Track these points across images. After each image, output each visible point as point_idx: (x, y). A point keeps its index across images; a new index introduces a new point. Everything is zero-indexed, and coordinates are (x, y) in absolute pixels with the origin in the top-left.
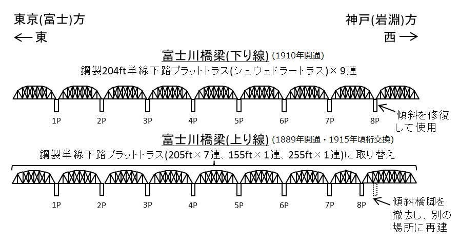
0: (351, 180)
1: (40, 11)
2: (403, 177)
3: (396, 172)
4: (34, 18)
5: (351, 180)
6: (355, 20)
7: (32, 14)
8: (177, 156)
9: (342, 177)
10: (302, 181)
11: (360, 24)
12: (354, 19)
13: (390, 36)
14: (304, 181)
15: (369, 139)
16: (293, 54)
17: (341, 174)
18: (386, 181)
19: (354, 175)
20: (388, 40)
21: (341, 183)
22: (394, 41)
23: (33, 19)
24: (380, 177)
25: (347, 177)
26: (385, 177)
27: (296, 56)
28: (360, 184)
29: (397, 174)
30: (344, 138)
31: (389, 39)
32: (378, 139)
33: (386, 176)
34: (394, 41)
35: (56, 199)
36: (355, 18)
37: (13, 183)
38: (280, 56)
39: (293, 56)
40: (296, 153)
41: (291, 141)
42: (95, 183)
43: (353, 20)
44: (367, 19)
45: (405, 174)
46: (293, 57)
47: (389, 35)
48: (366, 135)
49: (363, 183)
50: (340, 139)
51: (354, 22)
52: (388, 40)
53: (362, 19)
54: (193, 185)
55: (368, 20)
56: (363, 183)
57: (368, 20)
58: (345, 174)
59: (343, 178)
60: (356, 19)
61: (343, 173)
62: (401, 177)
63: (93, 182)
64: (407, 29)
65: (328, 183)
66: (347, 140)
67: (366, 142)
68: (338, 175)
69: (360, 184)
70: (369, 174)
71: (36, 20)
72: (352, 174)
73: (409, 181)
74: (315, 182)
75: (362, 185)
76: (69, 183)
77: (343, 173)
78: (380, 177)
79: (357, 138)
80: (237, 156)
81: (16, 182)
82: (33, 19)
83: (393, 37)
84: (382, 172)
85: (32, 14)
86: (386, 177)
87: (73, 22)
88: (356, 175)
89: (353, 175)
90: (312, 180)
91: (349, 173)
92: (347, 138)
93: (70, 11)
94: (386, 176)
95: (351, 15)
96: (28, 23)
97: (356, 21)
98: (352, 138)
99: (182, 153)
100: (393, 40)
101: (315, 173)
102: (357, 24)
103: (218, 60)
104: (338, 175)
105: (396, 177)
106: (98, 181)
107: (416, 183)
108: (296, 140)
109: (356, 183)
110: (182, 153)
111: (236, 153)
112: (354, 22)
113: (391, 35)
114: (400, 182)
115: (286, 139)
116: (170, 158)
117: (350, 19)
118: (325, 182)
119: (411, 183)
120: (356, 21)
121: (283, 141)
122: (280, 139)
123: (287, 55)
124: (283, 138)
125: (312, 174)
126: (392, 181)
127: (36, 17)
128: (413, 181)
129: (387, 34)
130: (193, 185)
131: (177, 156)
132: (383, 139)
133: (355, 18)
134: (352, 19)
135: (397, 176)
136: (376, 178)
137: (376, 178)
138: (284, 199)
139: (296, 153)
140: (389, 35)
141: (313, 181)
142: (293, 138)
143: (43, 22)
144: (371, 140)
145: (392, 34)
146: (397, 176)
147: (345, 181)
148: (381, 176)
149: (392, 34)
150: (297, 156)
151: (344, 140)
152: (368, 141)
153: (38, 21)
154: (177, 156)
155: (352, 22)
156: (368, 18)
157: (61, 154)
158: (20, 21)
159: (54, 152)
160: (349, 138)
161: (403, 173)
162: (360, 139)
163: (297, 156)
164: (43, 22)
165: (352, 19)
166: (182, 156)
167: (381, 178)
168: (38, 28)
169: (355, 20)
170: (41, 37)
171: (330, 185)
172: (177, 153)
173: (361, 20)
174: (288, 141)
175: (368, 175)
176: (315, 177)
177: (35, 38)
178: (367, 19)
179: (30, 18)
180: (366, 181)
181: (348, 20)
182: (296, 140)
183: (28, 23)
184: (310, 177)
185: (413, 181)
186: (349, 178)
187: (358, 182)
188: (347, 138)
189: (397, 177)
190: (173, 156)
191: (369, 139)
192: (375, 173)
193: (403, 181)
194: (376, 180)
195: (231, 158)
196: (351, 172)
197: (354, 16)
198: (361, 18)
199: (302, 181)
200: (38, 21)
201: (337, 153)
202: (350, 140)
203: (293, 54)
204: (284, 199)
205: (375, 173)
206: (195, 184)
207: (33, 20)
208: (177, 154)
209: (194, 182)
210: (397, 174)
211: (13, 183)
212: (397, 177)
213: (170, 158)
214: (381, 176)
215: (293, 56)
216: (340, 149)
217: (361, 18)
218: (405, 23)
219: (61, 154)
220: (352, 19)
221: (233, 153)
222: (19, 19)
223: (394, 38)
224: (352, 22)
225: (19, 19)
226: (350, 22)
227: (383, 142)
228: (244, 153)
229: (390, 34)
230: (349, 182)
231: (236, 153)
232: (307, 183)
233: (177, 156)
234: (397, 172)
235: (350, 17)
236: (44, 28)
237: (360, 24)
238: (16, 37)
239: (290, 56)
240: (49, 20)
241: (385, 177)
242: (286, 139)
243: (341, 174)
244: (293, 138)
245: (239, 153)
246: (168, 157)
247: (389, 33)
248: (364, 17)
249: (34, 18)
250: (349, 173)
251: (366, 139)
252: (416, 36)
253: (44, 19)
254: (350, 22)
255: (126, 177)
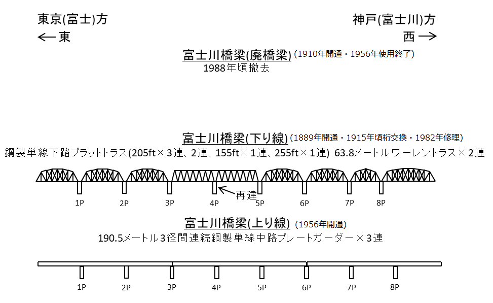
0: (370, 178)
1: (63, 11)
2: (422, 175)
3: (415, 170)
4: (58, 18)
5: (370, 178)
6: (362, 20)
7: (56, 14)
8: (140, 154)
9: (362, 176)
10: (322, 179)
11: (367, 24)
12: (361, 19)
13: (409, 36)
14: (324, 180)
15: (385, 137)
16: (315, 52)
17: (361, 172)
18: (405, 179)
19: (374, 173)
20: (407, 40)
21: (360, 181)
22: (413, 41)
23: (56, 18)
24: (399, 175)
25: (367, 175)
26: (404, 175)
27: (318, 54)
28: (380, 182)
29: (416, 172)
30: (361, 136)
31: (409, 39)
32: (395, 137)
33: (405, 174)
34: (413, 41)
35: (80, 197)
36: (362, 17)
37: (37, 181)
38: (302, 55)
39: (315, 55)
40: (283, 151)
41: (309, 139)
42: (118, 181)
43: (360, 20)
44: (373, 19)
45: (424, 172)
46: (315, 55)
47: (408, 35)
48: (383, 133)
49: (383, 181)
50: (357, 138)
51: (361, 21)
52: (407, 40)
53: (369, 19)
54: (124, 183)
55: (375, 20)
56: (383, 181)
57: (375, 20)
58: (365, 172)
59: (363, 176)
60: (363, 19)
61: (363, 172)
62: (420, 176)
63: (116, 180)
64: (427, 29)
65: (348, 182)
66: (364, 139)
67: (383, 140)
68: (358, 173)
69: (380, 182)
70: (388, 172)
71: (59, 19)
72: (372, 172)
73: (428, 179)
74: (335, 180)
75: (381, 183)
76: (92, 181)
77: (363, 172)
78: (399, 175)
79: (374, 136)
80: (224, 154)
81: (39, 180)
82: (56, 18)
83: (412, 36)
84: (401, 170)
85: (56, 14)
86: (405, 176)
87: (96, 22)
88: (376, 173)
89: (372, 173)
90: (332, 178)
91: (369, 172)
92: (364, 136)
93: (93, 11)
94: (405, 174)
95: (358, 14)
96: (51, 23)
97: (363, 21)
98: (370, 136)
99: (145, 151)
100: (412, 39)
101: (335, 172)
102: (364, 23)
103: (280, 60)
104: (358, 173)
105: (415, 175)
106: (120, 180)
107: (435, 181)
108: (314, 138)
109: (375, 181)
110: (145, 151)
111: (223, 151)
112: (361, 21)
113: (410, 35)
114: (419, 180)
115: (303, 137)
116: (133, 156)
117: (357, 19)
118: (345, 180)
119: (430, 181)
120: (363, 21)
121: (301, 139)
122: (298, 137)
123: (308, 54)
124: (301, 136)
125: (332, 172)
126: (411, 179)
127: (59, 17)
128: (432, 179)
129: (406, 33)
130: (124, 183)
131: (140, 154)
132: (399, 137)
133: (362, 17)
134: (359, 19)
135: (416, 174)
136: (395, 176)
137: (395, 176)
138: (305, 198)
139: (283, 151)
140: (408, 35)
141: (333, 179)
142: (311, 136)
143: (66, 22)
144: (388, 138)
145: (412, 33)
146: (416, 174)
147: (365, 179)
148: (400, 174)
149: (412, 33)
150: (283, 154)
151: (361, 138)
152: (385, 139)
153: (61, 21)
154: (140, 154)
155: (359, 21)
156: (375, 17)
157: (26, 152)
158: (43, 21)
159: (18, 150)
160: (366, 136)
161: (422, 172)
162: (377, 137)
163: (283, 154)
164: (66, 22)
165: (359, 19)
166: (146, 154)
167: (400, 176)
168: (61, 28)
169: (362, 20)
170: (65, 36)
171: (349, 183)
172: (140, 151)
173: (368, 20)
174: (306, 139)
175: (387, 173)
176: (335, 175)
177: (59, 38)
178: (373, 19)
179: (54, 18)
180: (385, 179)
181: (355, 20)
182: (314, 138)
183: (51, 23)
184: (330, 175)
185: (432, 179)
186: (369, 176)
187: (377, 180)
188: (364, 136)
189: (416, 176)
190: (136, 154)
191: (385, 137)
192: (395, 171)
193: (422, 179)
194: (395, 178)
195: (218, 156)
196: (371, 171)
197: (361, 16)
198: (368, 17)
199: (322, 179)
200: (61, 21)
201: (323, 151)
202: (367, 138)
203: (315, 53)
204: (305, 198)
205: (395, 171)
206: (126, 182)
207: (56, 20)
208: (140, 152)
209: (125, 180)
210: (416, 172)
211: (37, 181)
212: (416, 176)
213: (133, 156)
214: (400, 174)
215: (315, 55)
216: (325, 147)
217: (368, 17)
218: (424, 23)
219: (26, 152)
220: (359, 19)
221: (220, 151)
222: (43, 19)
223: (413, 38)
224: (359, 21)
225: (43, 19)
226: (357, 22)
227: (399, 140)
228: (231, 151)
229: (409, 33)
230: (369, 180)
231: (223, 151)
232: (327, 181)
233: (140, 154)
234: (416, 171)
235: (357, 16)
236: (68, 28)
237: (367, 24)
238: (40, 37)
239: (312, 55)
240: (73, 20)
241: (404, 175)
242: (303, 137)
243: (361, 172)
244: (311, 136)
245: (226, 151)
246: (131, 155)
247: (408, 32)
248: (371, 17)
249: (58, 18)
250: (369, 172)
251: (383, 137)
252: (435, 36)
253: (67, 19)
254: (357, 22)
255: (102, 175)
